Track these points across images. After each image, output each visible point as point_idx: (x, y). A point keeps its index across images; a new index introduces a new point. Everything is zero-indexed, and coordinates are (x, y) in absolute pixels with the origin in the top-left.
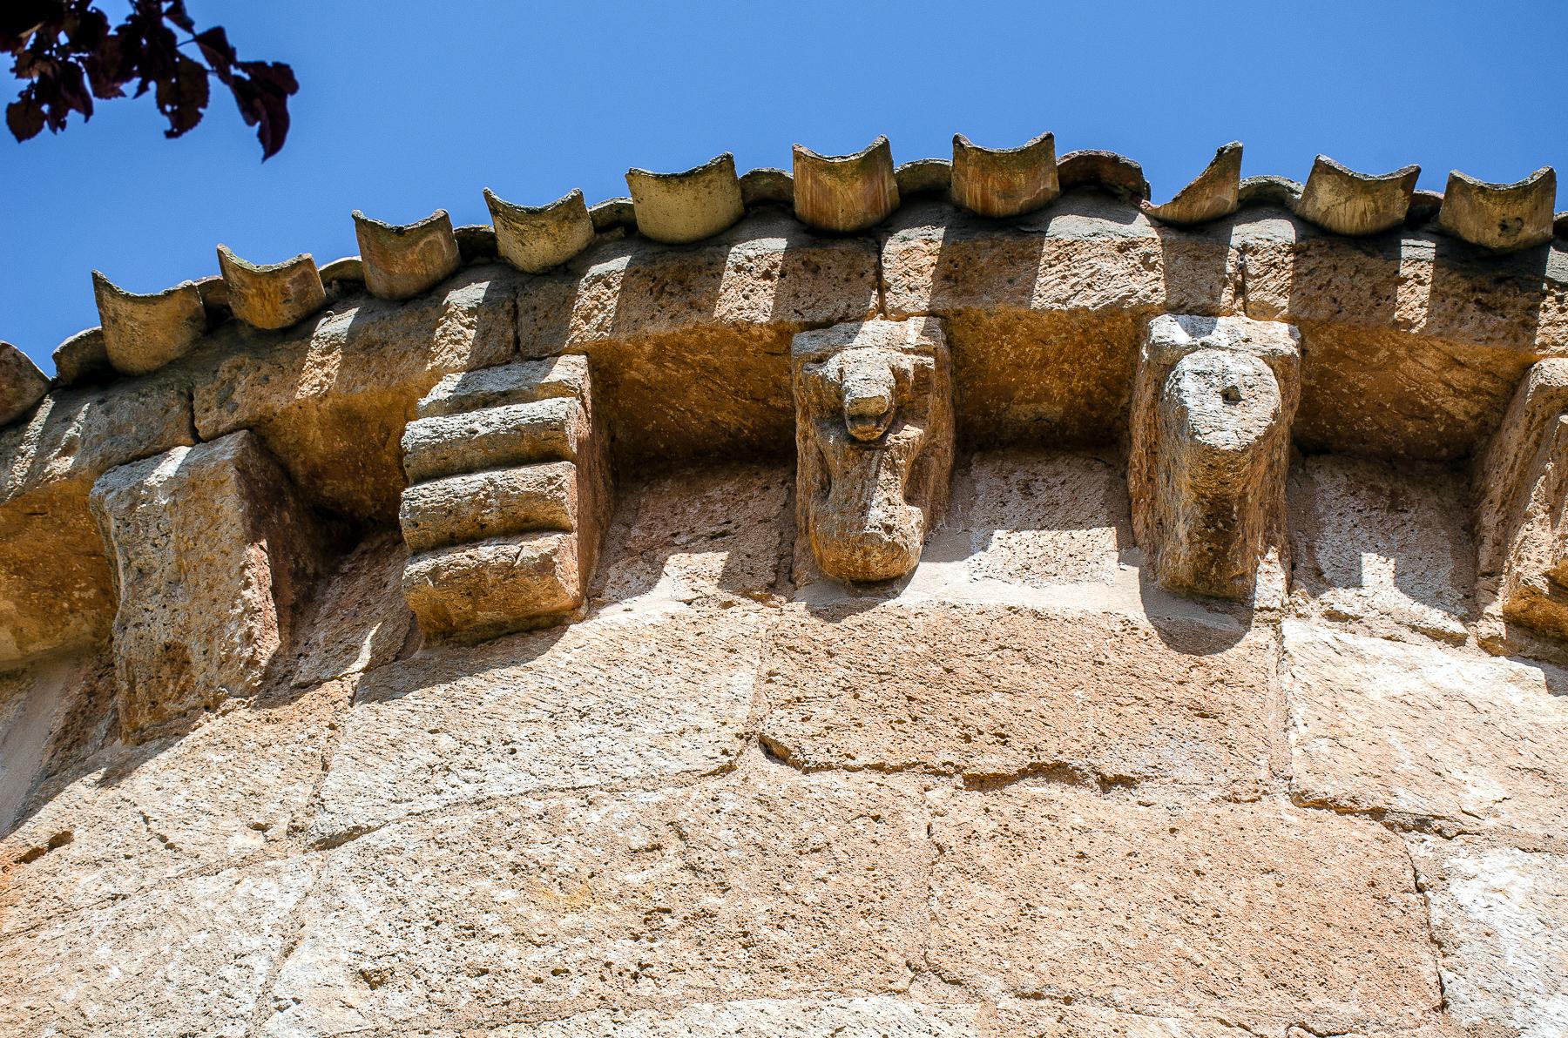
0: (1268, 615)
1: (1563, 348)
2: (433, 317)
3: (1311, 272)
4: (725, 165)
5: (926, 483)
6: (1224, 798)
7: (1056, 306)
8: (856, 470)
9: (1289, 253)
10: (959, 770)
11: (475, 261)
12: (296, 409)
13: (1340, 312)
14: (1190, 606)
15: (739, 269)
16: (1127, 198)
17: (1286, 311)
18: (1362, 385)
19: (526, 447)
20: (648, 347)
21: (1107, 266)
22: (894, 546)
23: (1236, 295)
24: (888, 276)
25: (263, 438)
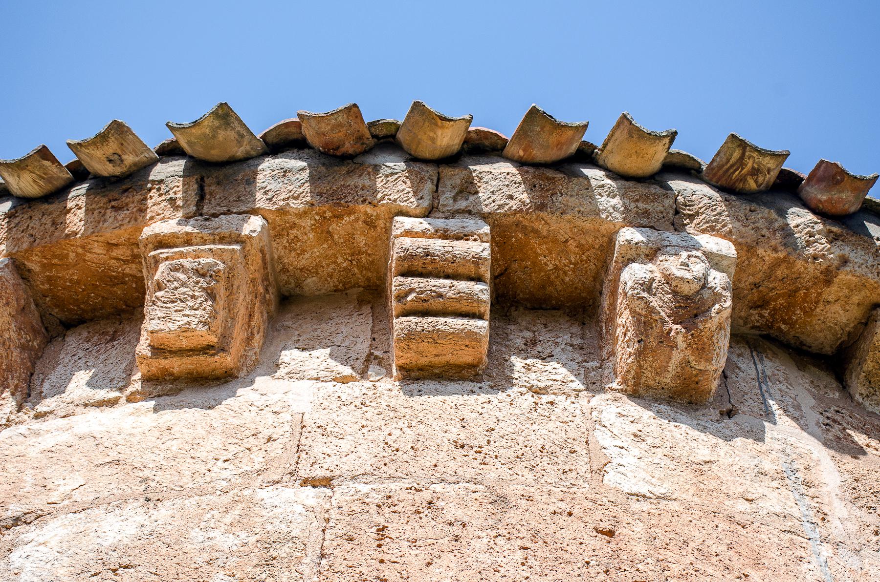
1: (163, 215)
3: (17, 225)
9: (5, 218)
13: (35, 241)
18: (75, 277)
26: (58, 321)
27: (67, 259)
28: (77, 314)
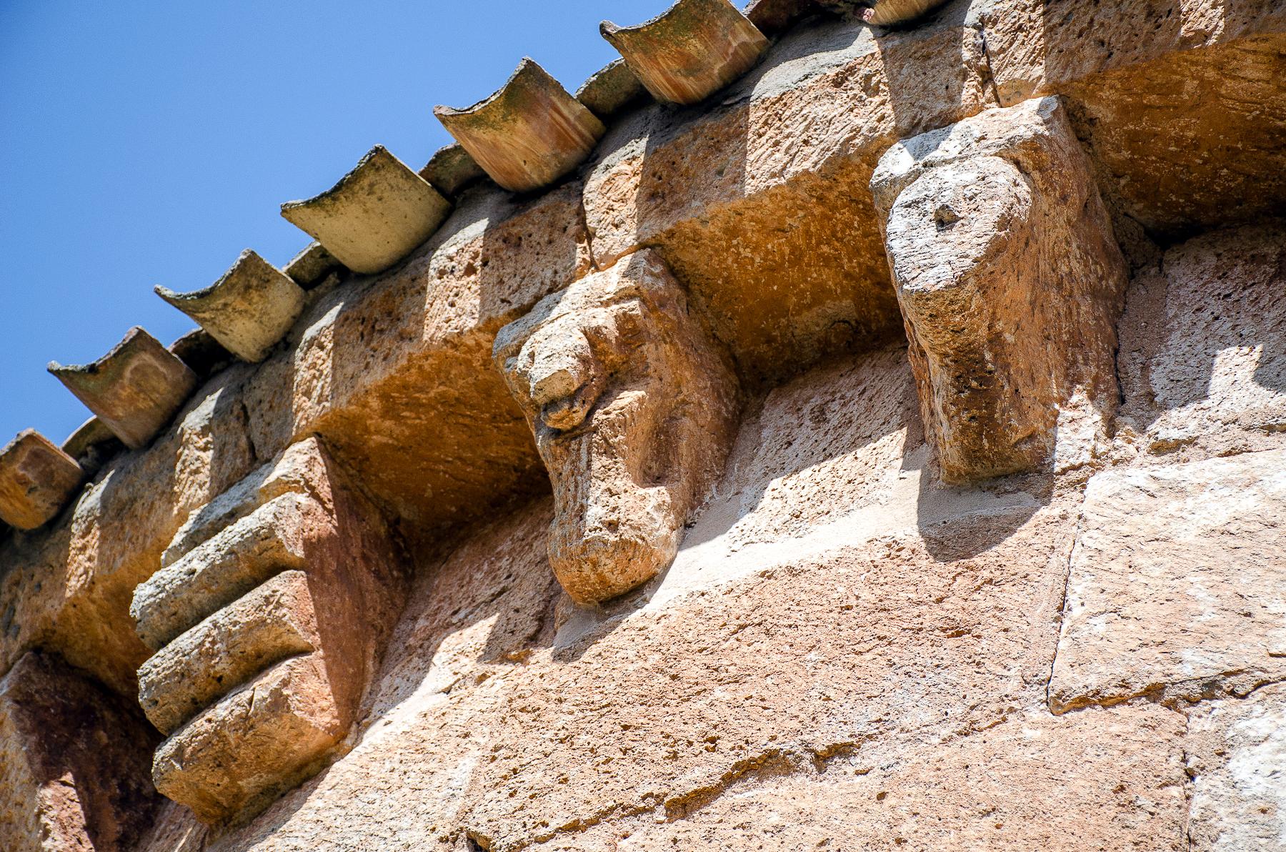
0: (1074, 476)
2: (171, 451)
3: (1066, 19)
4: (379, 161)
5: (676, 453)
6: (960, 734)
7: (772, 182)
8: (567, 468)
10: (659, 799)
11: (213, 369)
12: (71, 610)
14: (976, 498)
15: (442, 273)
16: (850, 15)
17: (1043, 80)
18: (1191, 134)
19: (245, 569)
20: (375, 403)
21: (822, 109)
22: (623, 545)
23: (984, 84)
24: (591, 220)
25: (58, 654)
26: (1141, 229)
27: (1180, 93)
28: (1182, 214)
